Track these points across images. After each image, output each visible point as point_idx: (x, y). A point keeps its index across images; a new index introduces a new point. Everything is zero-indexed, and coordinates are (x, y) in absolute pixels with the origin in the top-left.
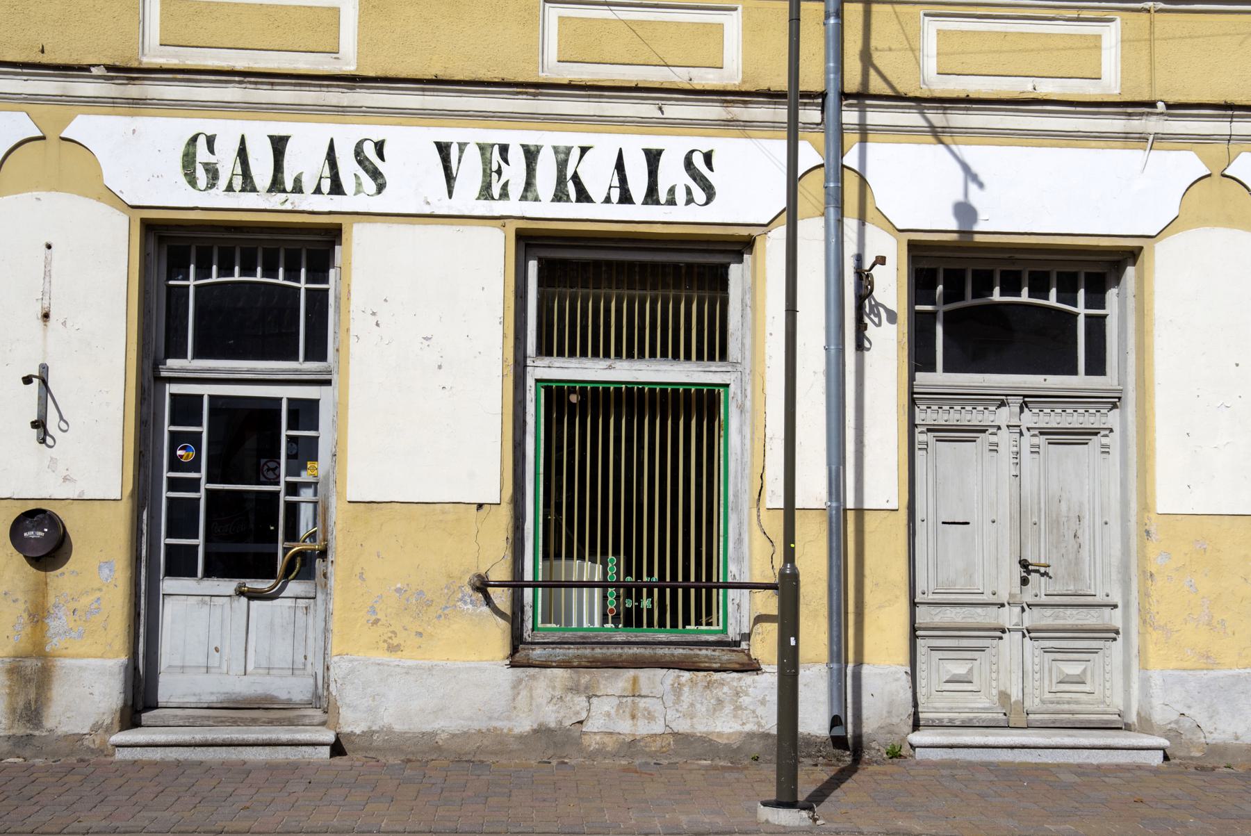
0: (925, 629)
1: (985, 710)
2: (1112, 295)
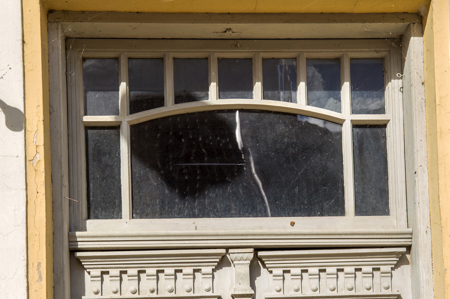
2: (393, 87)
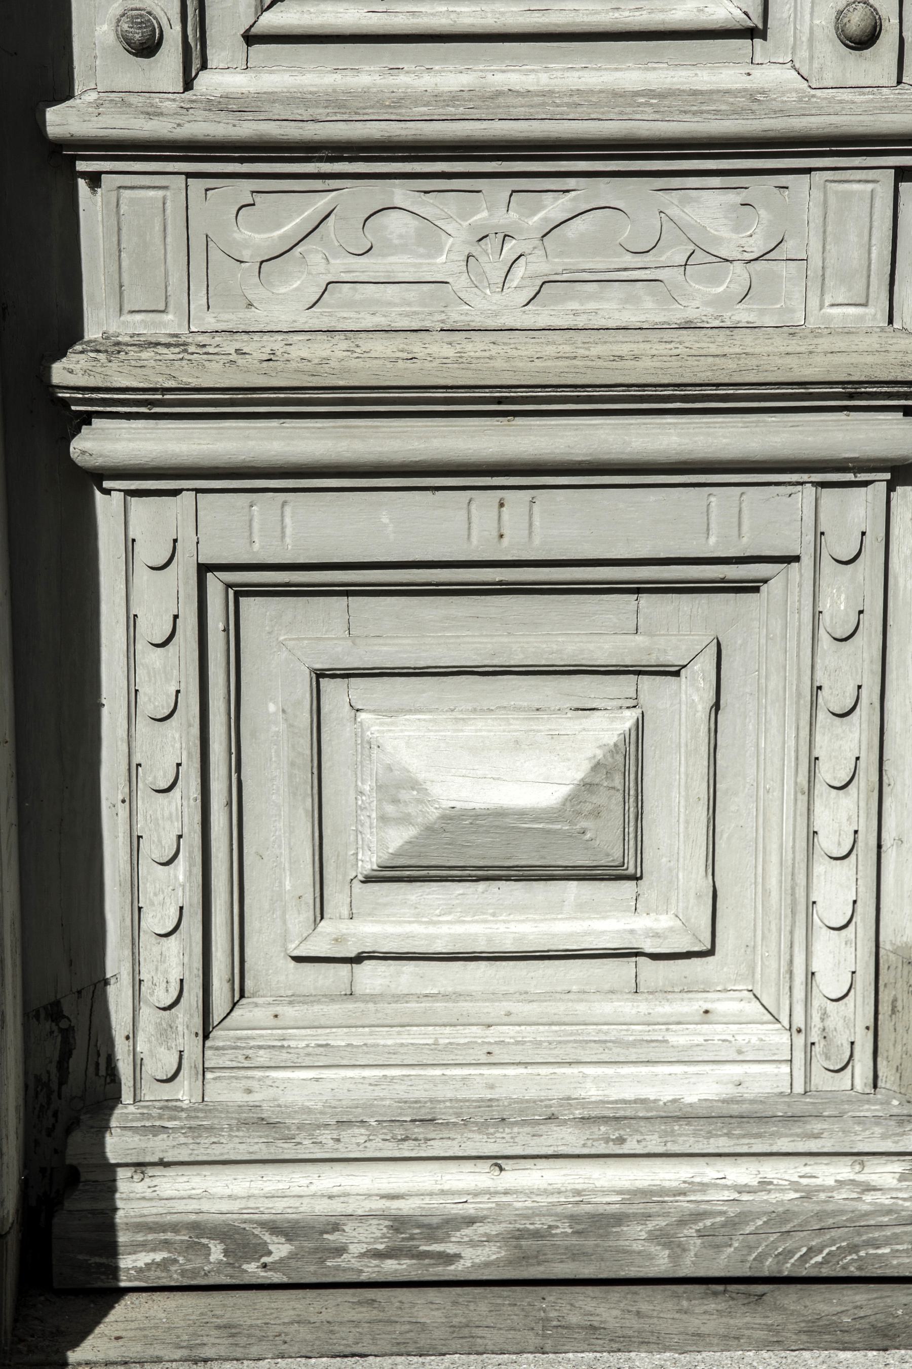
0: (153, 405)
1: (740, 1123)
